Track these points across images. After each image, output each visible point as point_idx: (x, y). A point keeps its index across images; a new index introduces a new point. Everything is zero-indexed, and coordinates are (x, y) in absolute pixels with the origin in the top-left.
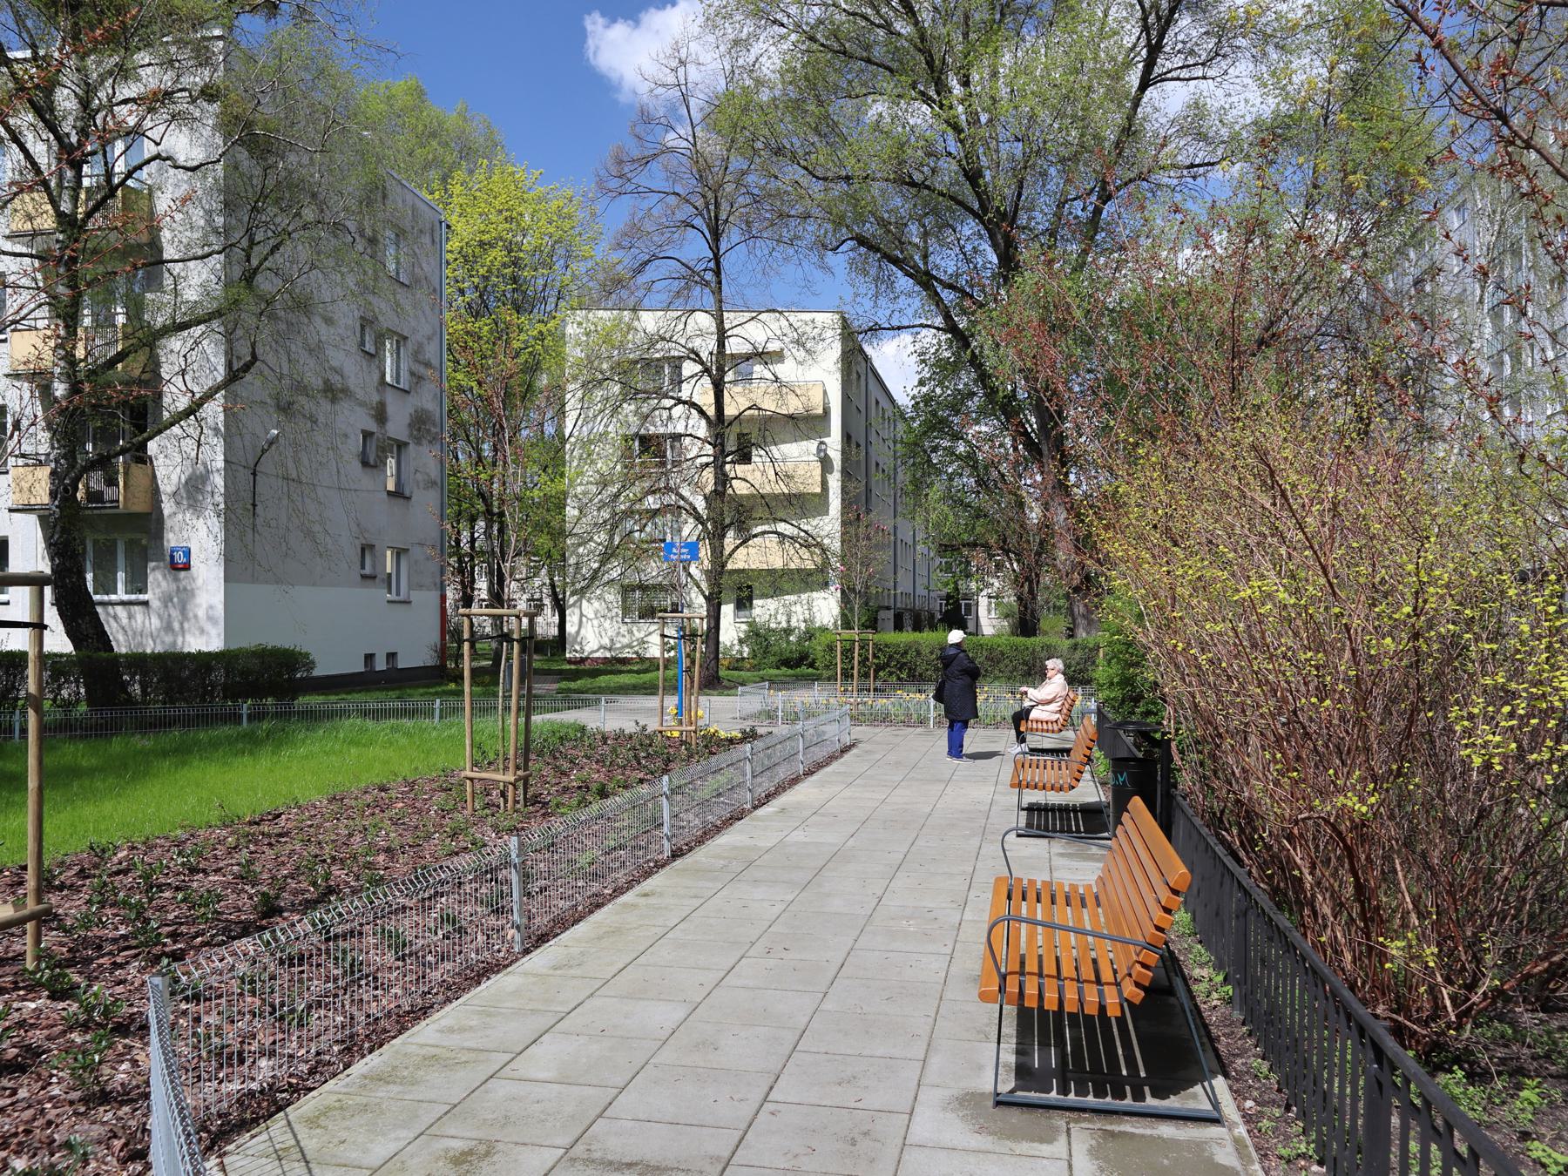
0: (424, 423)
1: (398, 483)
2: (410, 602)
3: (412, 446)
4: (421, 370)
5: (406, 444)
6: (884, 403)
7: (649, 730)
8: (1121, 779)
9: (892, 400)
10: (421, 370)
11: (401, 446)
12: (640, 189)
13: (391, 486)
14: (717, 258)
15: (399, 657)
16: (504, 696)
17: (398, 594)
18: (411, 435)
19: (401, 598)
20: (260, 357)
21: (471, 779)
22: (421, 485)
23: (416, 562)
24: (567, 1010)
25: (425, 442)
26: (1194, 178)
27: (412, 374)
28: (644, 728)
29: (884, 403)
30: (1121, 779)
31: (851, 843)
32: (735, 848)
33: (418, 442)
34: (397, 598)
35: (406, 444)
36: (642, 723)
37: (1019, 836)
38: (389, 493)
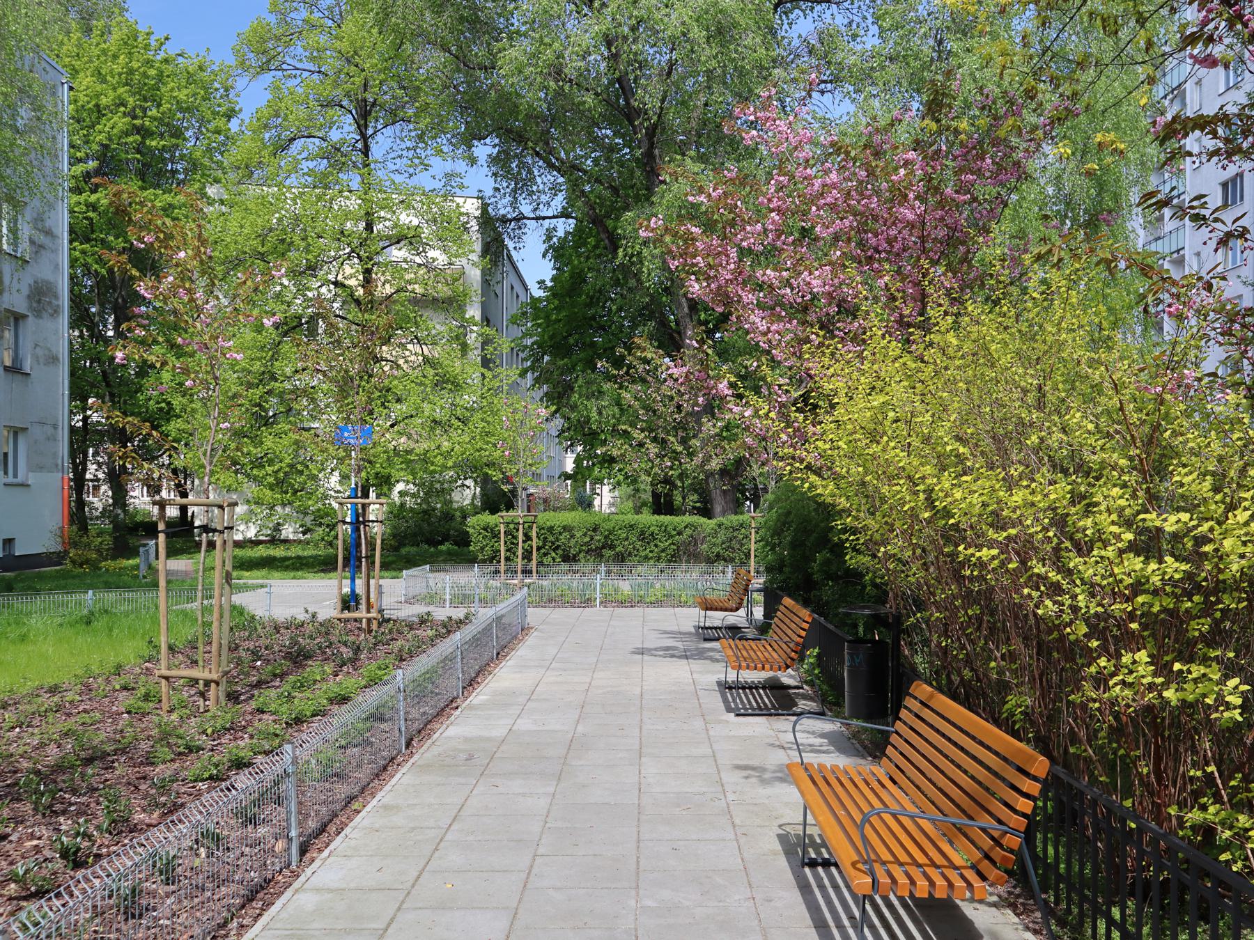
0: (44, 294)
1: (16, 358)
2: (28, 486)
3: (31, 319)
4: (42, 239)
5: (24, 317)
6: (518, 288)
7: (321, 617)
8: (857, 661)
9: (526, 289)
10: (42, 239)
11: (18, 318)
12: (284, 66)
13: (8, 363)
14: (365, 138)
15: (17, 543)
16: (196, 590)
17: (15, 476)
18: (30, 308)
19: (20, 480)
20: (1213, 370)
21: (167, 678)
22: (41, 360)
23: (36, 442)
24: (383, 926)
25: (45, 315)
26: (822, 93)
27: (32, 242)
28: (314, 616)
29: (518, 288)
30: (857, 661)
31: (580, 728)
32: (467, 740)
33: (38, 313)
34: (15, 481)
35: (24, 317)
36: (311, 610)
37: (738, 715)
38: (6, 369)
